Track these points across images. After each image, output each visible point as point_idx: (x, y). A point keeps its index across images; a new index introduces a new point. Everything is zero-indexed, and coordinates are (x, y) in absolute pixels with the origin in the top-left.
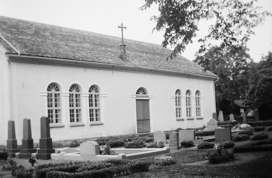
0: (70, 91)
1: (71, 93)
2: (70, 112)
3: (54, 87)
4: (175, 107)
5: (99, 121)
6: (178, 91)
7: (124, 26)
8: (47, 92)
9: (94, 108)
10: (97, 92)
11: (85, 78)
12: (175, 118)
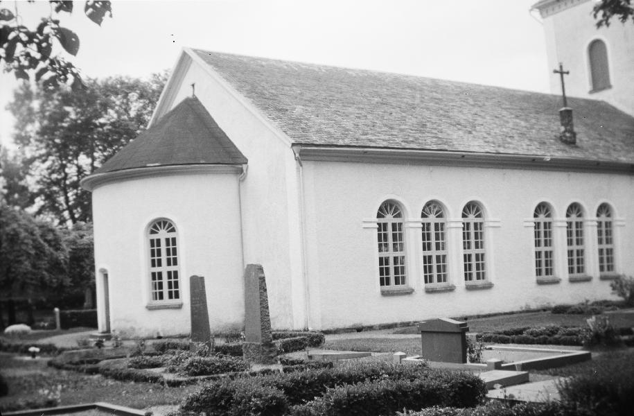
0: (379, 216)
1: (382, 221)
2: (381, 263)
3: (390, 209)
4: (533, 249)
5: (483, 278)
6: (543, 208)
7: (565, 70)
8: (377, 220)
9: (434, 253)
10: (549, 216)
11: (453, 189)
12: (534, 278)
